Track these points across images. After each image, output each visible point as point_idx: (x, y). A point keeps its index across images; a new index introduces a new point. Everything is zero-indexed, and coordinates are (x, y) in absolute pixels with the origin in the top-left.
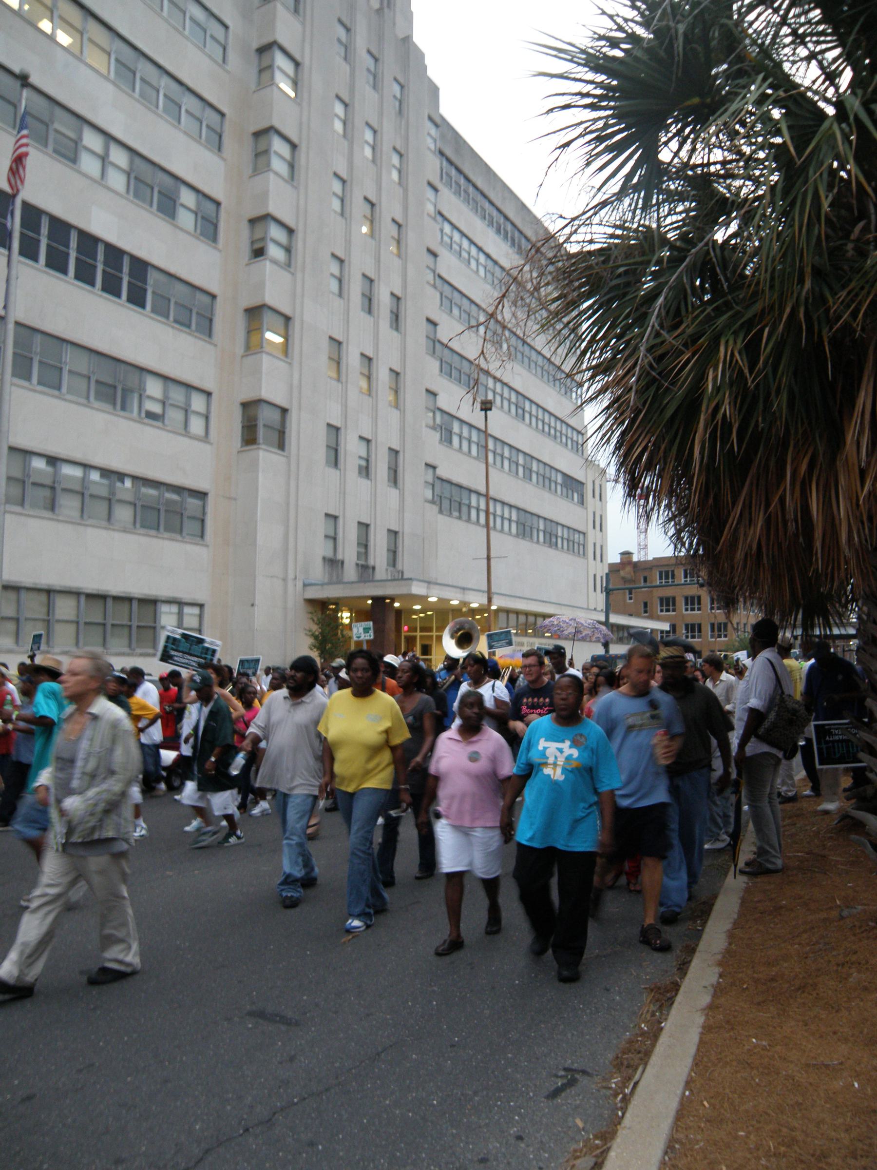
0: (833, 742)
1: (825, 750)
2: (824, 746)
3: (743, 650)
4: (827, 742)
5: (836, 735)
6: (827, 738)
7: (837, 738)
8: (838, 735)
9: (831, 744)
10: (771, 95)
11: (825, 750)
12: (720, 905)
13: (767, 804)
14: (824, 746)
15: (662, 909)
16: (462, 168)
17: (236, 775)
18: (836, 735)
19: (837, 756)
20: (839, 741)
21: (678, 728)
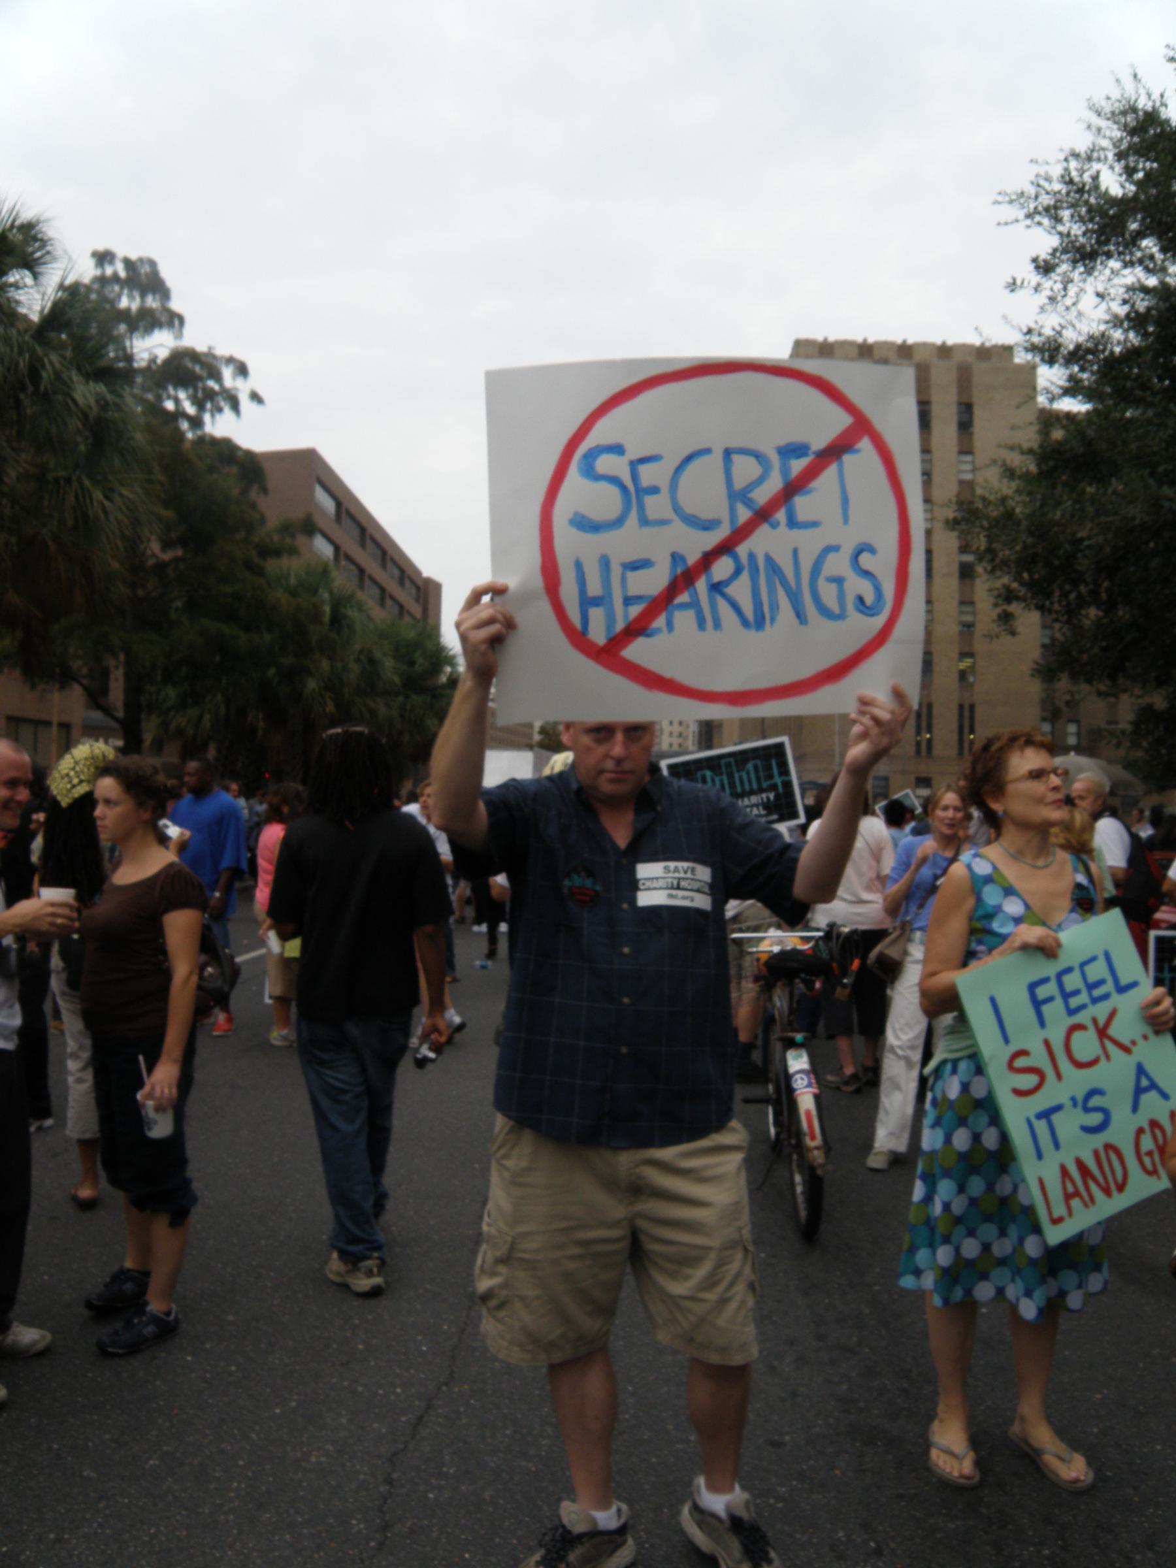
0: (761, 790)
1: (775, 771)
2: (778, 780)
3: (978, 1463)
4: (773, 788)
5: (757, 806)
6: (772, 796)
7: (754, 799)
8: (752, 806)
9: (765, 785)
10: (613, 1539)
11: (775, 771)
12: (453, 711)
13: (853, 878)
14: (778, 780)
15: (561, 728)
16: (252, 850)
17: (496, 873)
18: (757, 806)
19: (750, 766)
20: (752, 792)
21: (46, 311)
